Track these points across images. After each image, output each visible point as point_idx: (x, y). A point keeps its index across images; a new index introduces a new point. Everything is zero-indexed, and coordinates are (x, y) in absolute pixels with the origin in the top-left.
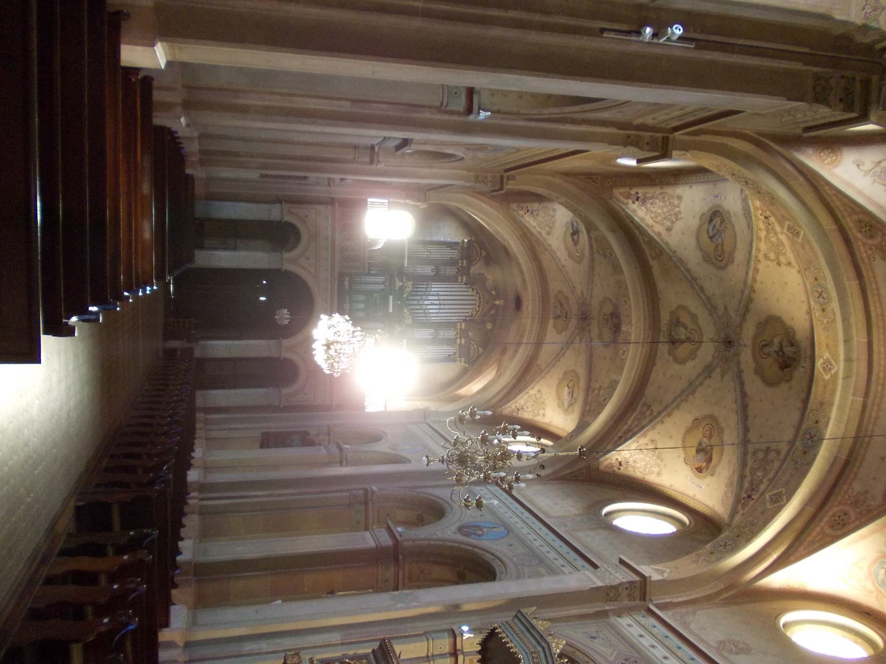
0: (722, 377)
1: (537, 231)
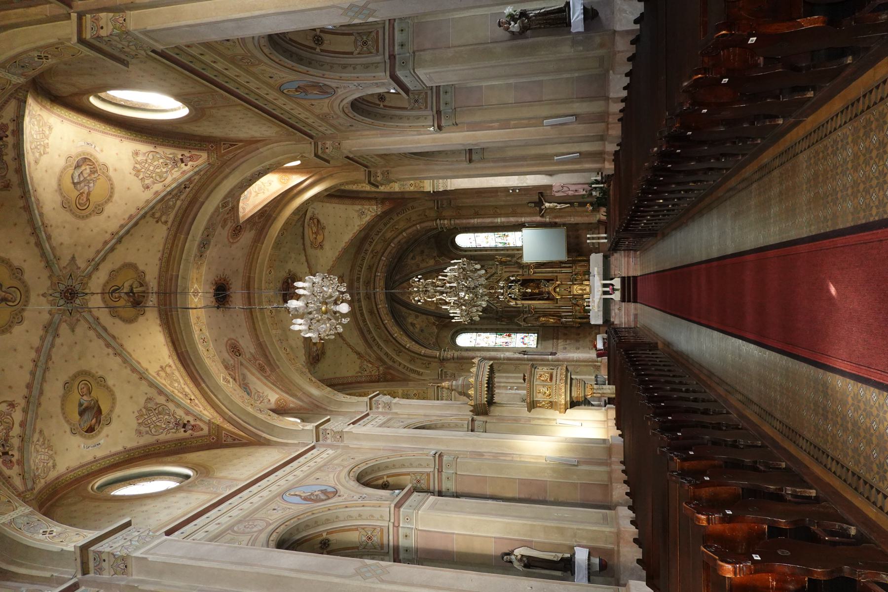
0: (73, 331)
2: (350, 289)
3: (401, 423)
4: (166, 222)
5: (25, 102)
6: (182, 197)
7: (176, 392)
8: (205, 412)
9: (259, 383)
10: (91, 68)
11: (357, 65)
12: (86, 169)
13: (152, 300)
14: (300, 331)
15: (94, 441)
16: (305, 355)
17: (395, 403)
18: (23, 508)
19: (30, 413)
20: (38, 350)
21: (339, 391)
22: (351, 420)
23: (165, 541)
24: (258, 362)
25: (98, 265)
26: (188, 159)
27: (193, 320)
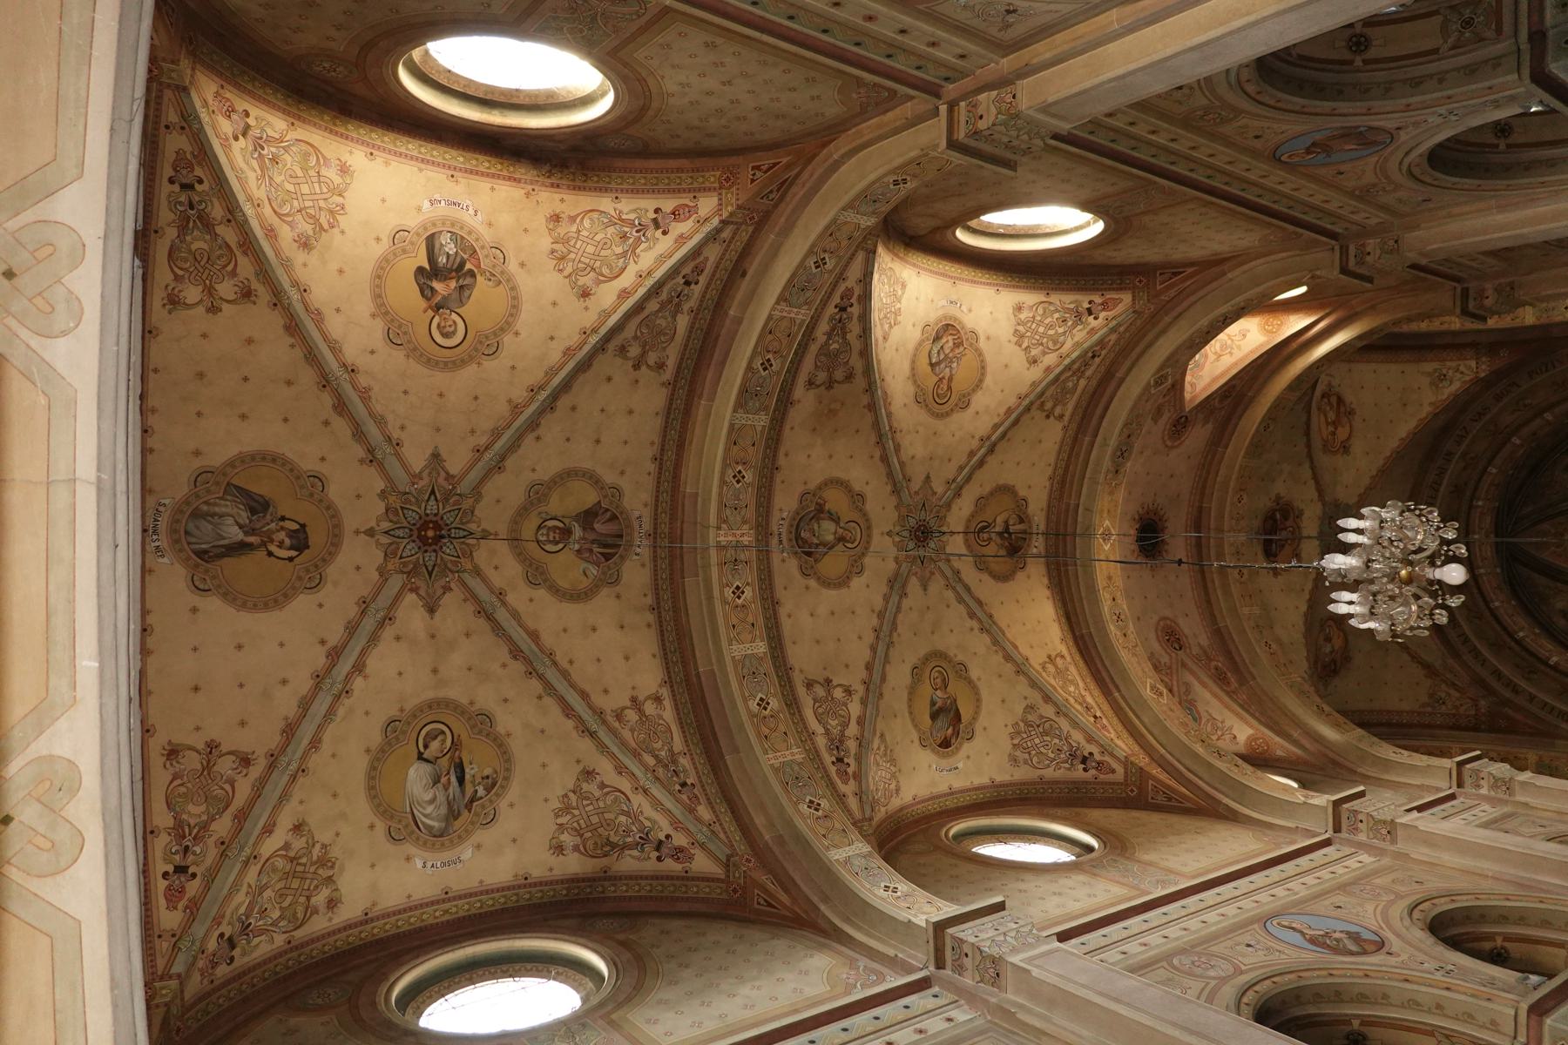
0: (925, 590)
1: (259, 216)
2: (1464, 536)
3: (1542, 829)
4: (1061, 416)
5: (875, 252)
6: (1089, 373)
7: (1072, 701)
8: (1119, 742)
9: (1214, 702)
10: (960, 184)
11: (1447, 72)
12: (947, 341)
13: (1038, 545)
14: (1351, 616)
15: (950, 762)
16: (1308, 659)
17: (1523, 784)
18: (860, 845)
19: (870, 706)
20: (881, 615)
21: (1381, 737)
22: (1411, 801)
23: (1057, 950)
24: (1214, 663)
25: (961, 488)
26: (1100, 308)
27: (1101, 582)
